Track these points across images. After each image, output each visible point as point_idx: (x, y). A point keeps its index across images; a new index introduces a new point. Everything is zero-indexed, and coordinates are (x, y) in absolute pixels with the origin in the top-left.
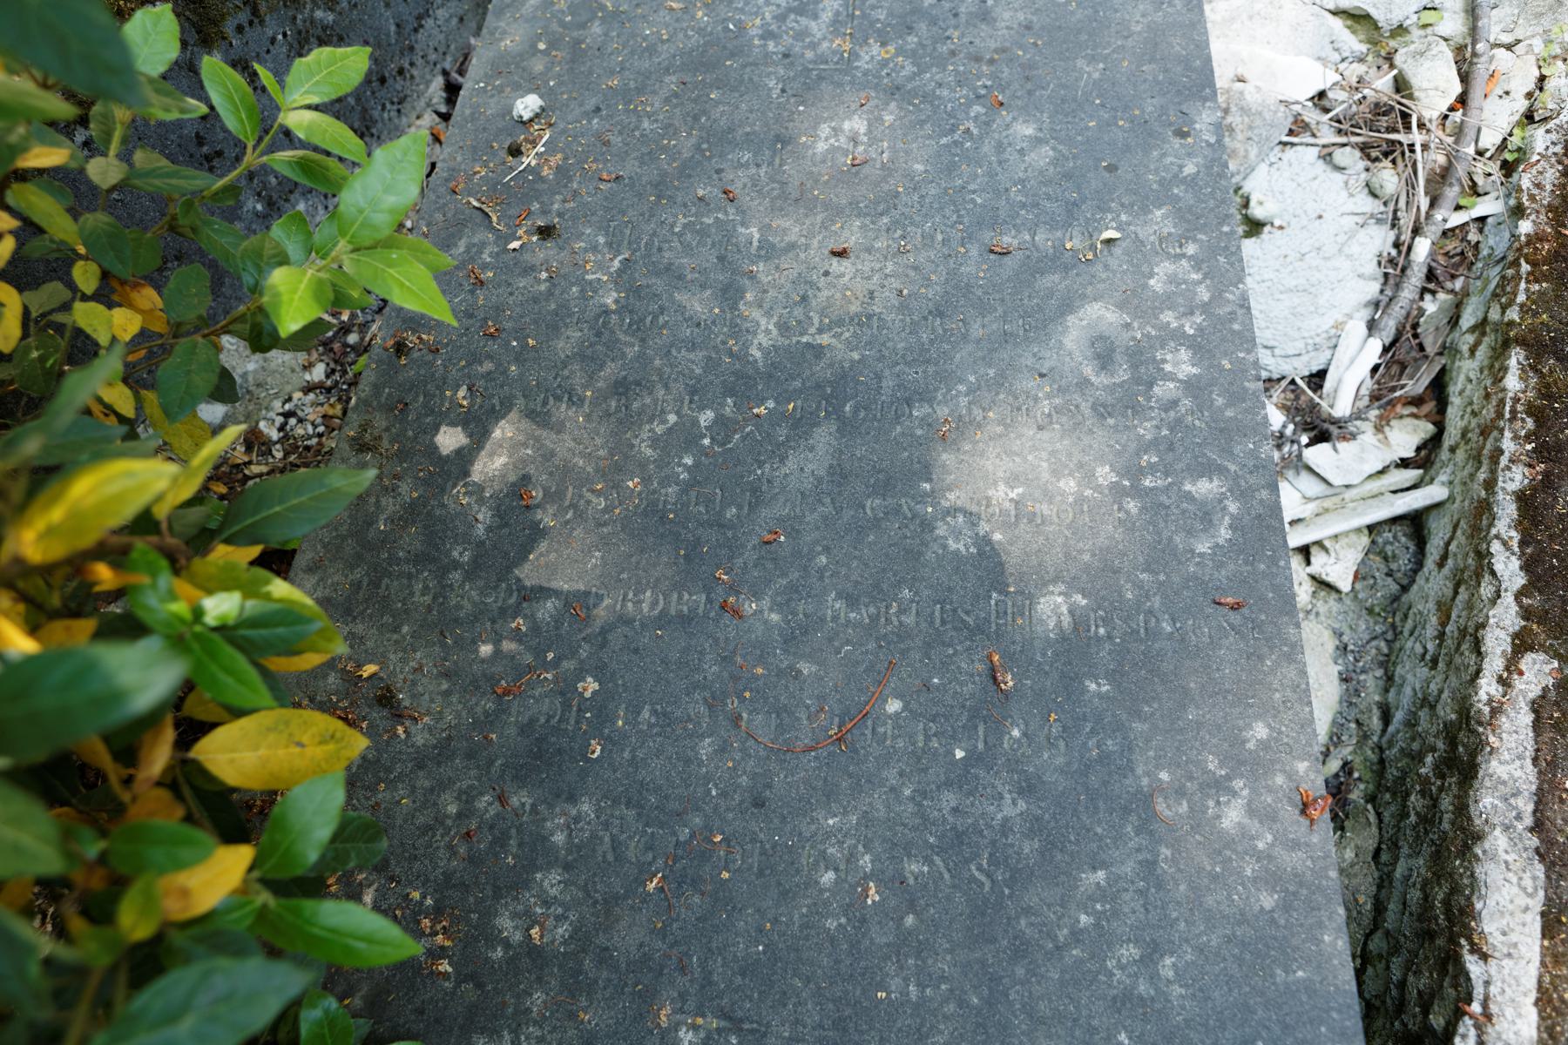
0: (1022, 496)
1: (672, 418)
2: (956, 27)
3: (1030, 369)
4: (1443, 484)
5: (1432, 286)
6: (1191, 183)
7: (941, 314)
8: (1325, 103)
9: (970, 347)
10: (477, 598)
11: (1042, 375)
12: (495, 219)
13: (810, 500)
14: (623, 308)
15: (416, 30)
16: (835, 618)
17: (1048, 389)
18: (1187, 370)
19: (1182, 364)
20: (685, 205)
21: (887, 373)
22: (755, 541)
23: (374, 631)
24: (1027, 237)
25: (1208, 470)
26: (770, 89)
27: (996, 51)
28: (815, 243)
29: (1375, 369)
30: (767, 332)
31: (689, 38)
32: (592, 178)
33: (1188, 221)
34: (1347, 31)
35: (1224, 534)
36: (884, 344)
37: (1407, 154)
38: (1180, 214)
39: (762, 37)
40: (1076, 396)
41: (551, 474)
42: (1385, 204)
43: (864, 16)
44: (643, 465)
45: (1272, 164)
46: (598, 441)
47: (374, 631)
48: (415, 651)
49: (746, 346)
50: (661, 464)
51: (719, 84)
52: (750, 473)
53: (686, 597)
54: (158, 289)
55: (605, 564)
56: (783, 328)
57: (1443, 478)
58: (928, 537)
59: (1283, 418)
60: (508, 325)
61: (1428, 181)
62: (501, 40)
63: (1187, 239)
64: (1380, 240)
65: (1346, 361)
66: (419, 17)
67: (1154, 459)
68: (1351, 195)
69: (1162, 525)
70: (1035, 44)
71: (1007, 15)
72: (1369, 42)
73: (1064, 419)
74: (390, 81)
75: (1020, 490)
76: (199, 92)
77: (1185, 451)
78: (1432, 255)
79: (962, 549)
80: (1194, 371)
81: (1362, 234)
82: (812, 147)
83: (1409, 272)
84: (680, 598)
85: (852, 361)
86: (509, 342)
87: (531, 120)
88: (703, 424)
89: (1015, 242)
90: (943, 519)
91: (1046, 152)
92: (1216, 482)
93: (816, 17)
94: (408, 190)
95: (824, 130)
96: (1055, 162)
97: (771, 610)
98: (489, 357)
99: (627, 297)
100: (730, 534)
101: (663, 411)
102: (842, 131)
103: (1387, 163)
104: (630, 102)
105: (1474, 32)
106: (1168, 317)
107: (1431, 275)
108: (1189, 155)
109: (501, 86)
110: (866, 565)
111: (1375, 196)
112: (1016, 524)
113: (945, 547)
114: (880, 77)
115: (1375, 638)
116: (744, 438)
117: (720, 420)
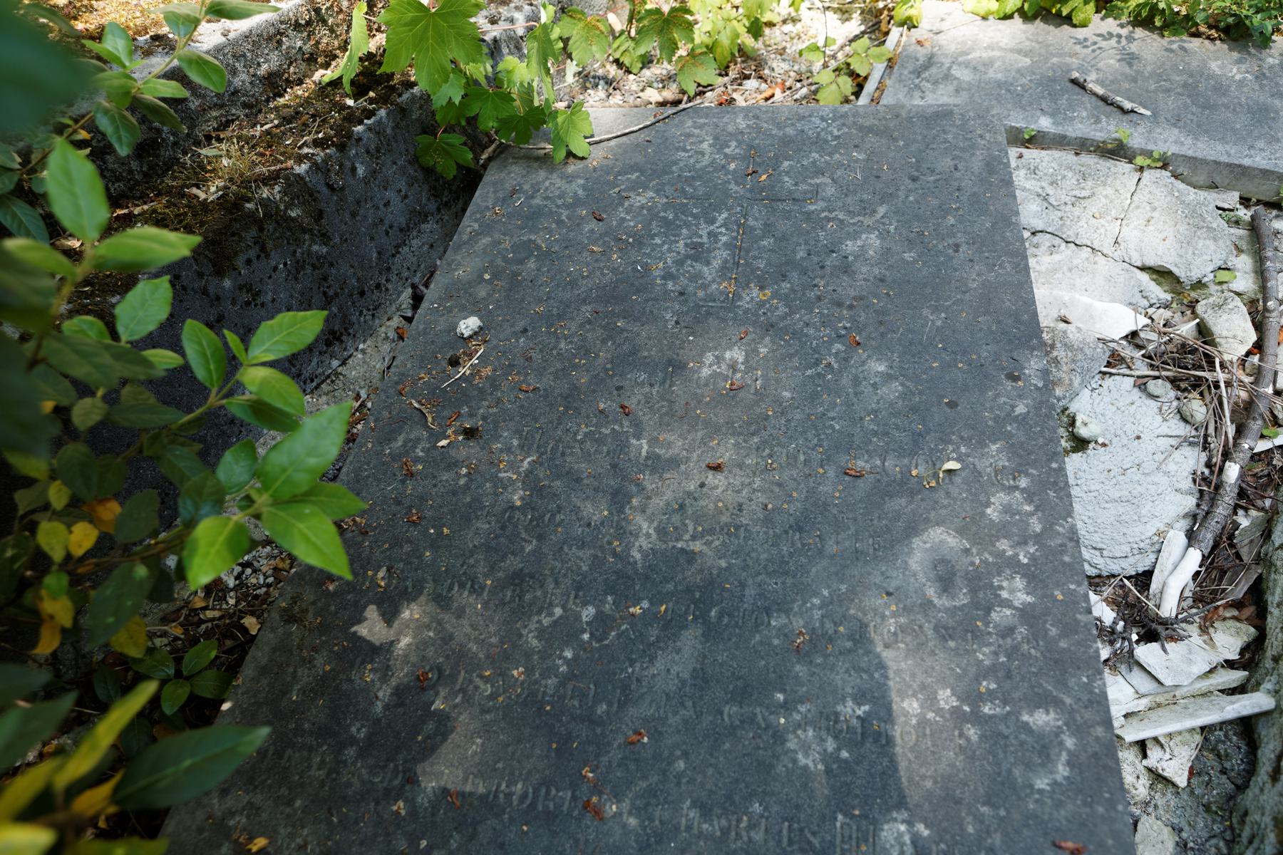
0: (867, 713)
1: (558, 611)
2: (822, 277)
3: (879, 587)
4: (1269, 692)
5: (1243, 503)
6: (1022, 421)
7: (800, 529)
8: (1137, 341)
9: (825, 563)
10: (366, 776)
11: (889, 594)
12: (430, 419)
13: (673, 703)
14: (528, 505)
15: (393, 256)
16: (689, 828)
17: (893, 608)
18: (1022, 598)
19: (1017, 592)
20: (588, 417)
21: (750, 582)
22: (621, 739)
23: (270, 802)
24: (878, 462)
25: (1044, 701)
26: (667, 321)
27: (855, 298)
28: (695, 456)
29: (1197, 573)
30: (648, 535)
31: (604, 275)
32: (513, 388)
33: (1021, 457)
34: (1153, 283)
35: (1062, 770)
36: (748, 554)
37: (1213, 391)
38: (1013, 449)
39: (663, 278)
40: (919, 617)
41: (447, 657)
42: (1196, 429)
43: (747, 264)
44: (528, 655)
45: (1093, 390)
46: (492, 629)
47: (270, 802)
48: (303, 827)
49: (628, 547)
50: (545, 655)
51: (625, 315)
52: (622, 670)
53: (553, 792)
54: (121, 504)
55: (484, 752)
56: (662, 532)
57: (1268, 685)
58: (779, 749)
59: (1114, 615)
60: (429, 514)
61: (1233, 412)
62: (456, 270)
63: (1020, 472)
64: (1192, 460)
65: (1170, 567)
66: (398, 246)
67: (993, 686)
68: (1165, 420)
69: (1001, 756)
70: (888, 294)
71: (864, 269)
72: (1172, 292)
73: (909, 639)
74: (369, 294)
75: (866, 708)
76: (177, 347)
77: (1023, 680)
78: (1242, 476)
79: (811, 765)
80: (1029, 599)
81: (1177, 454)
82: (698, 371)
83: (1221, 491)
84: (548, 793)
85: (720, 568)
86: (428, 529)
87: (471, 337)
88: (584, 619)
89: (868, 466)
90: (794, 732)
91: (896, 386)
92: (1052, 715)
93: (708, 263)
94: (331, 447)
95: (709, 358)
96: (903, 396)
97: (630, 813)
98: (409, 541)
99: (531, 495)
100: (599, 731)
101: (551, 604)
102: (724, 359)
103: (1195, 394)
104: (552, 325)
105: (1263, 288)
106: (1003, 545)
107: (1242, 494)
108: (1020, 397)
109: (451, 307)
110: (720, 773)
111: (1186, 421)
112: (862, 743)
113: (795, 761)
114: (757, 315)
115: (1214, 837)
116: (619, 636)
117: (600, 617)
